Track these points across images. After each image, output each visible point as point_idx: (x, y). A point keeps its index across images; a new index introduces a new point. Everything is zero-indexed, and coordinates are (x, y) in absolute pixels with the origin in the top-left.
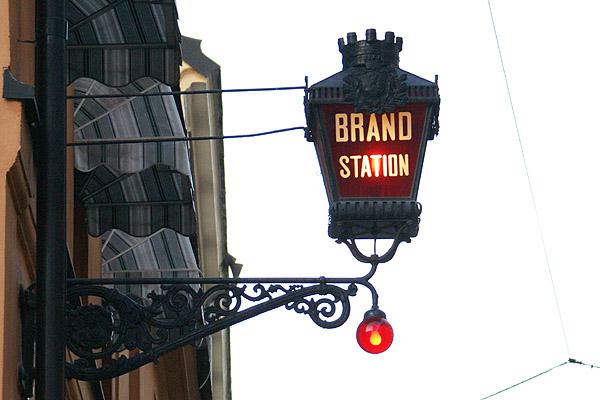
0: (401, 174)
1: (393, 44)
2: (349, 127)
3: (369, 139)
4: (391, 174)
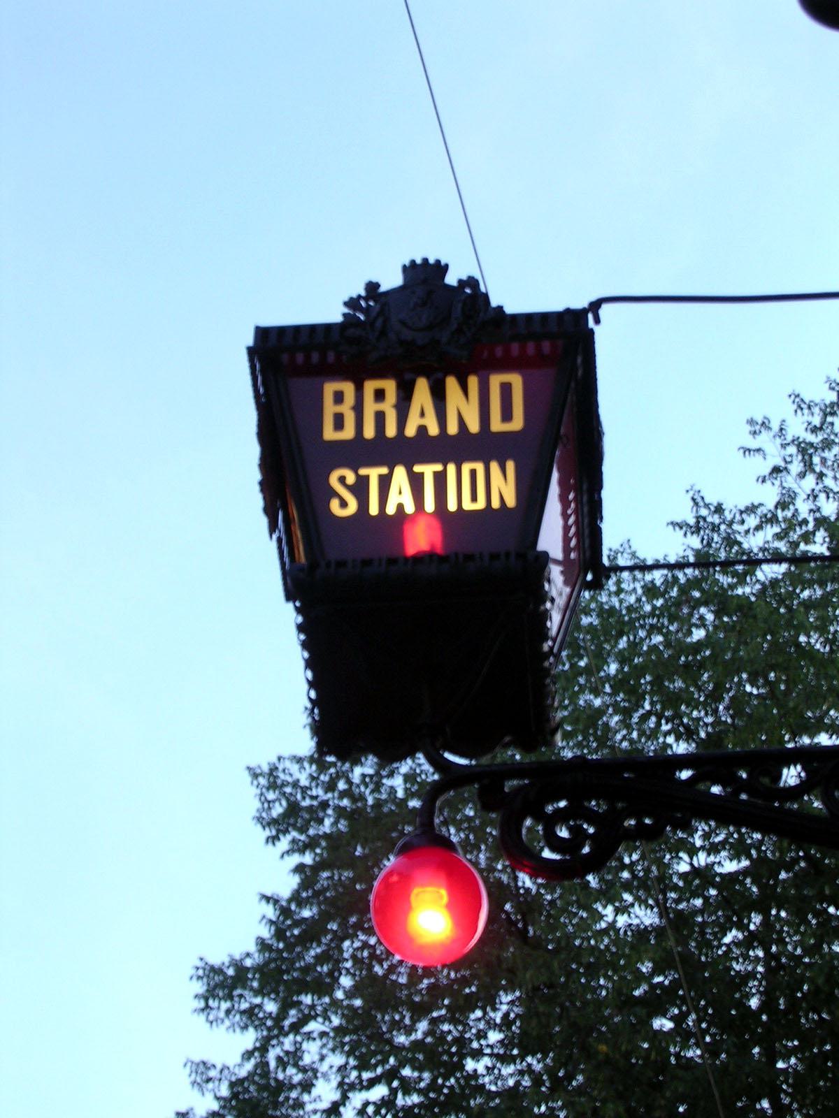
0: (496, 504)
1: (722, 504)
2: (358, 409)
3: (410, 431)
4: (468, 505)
